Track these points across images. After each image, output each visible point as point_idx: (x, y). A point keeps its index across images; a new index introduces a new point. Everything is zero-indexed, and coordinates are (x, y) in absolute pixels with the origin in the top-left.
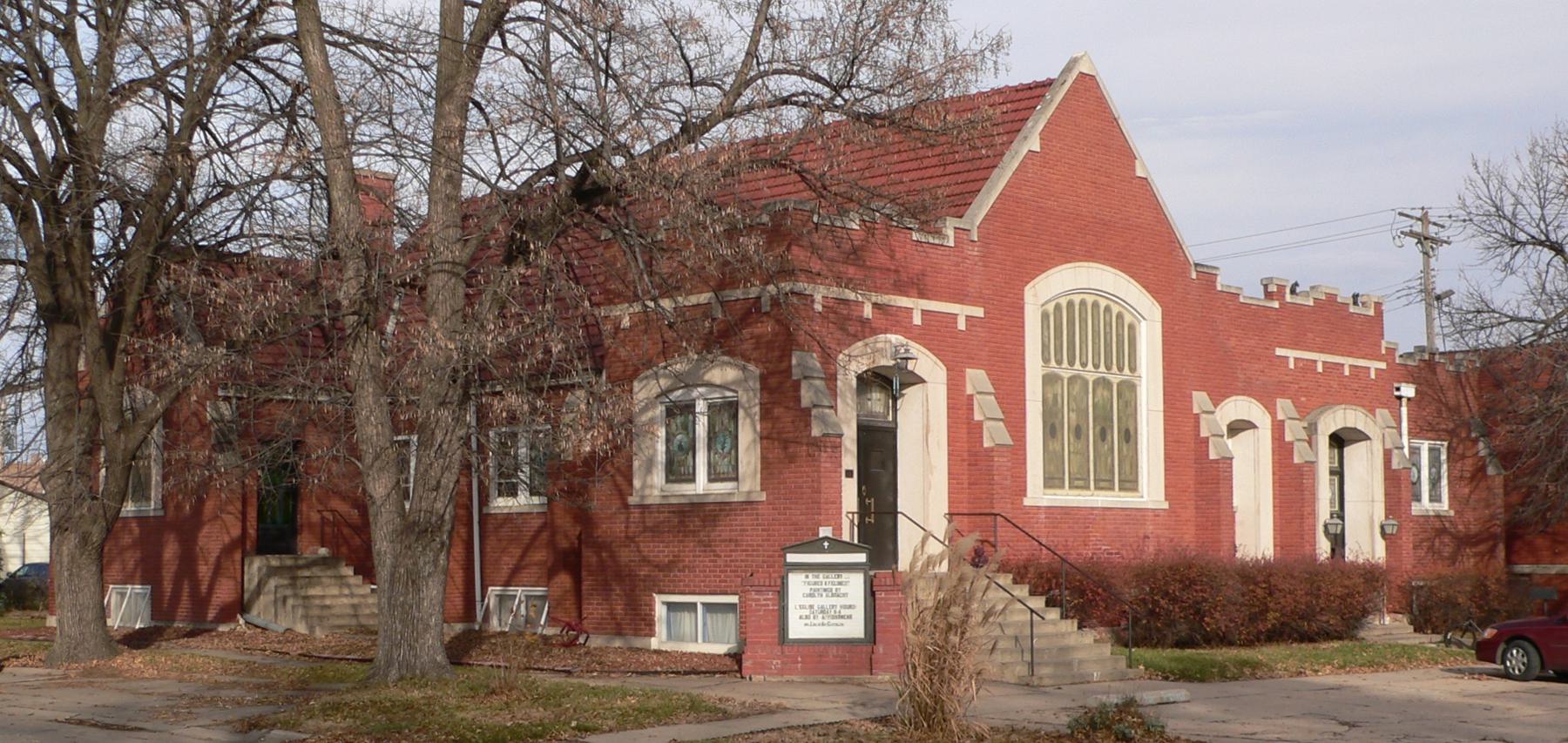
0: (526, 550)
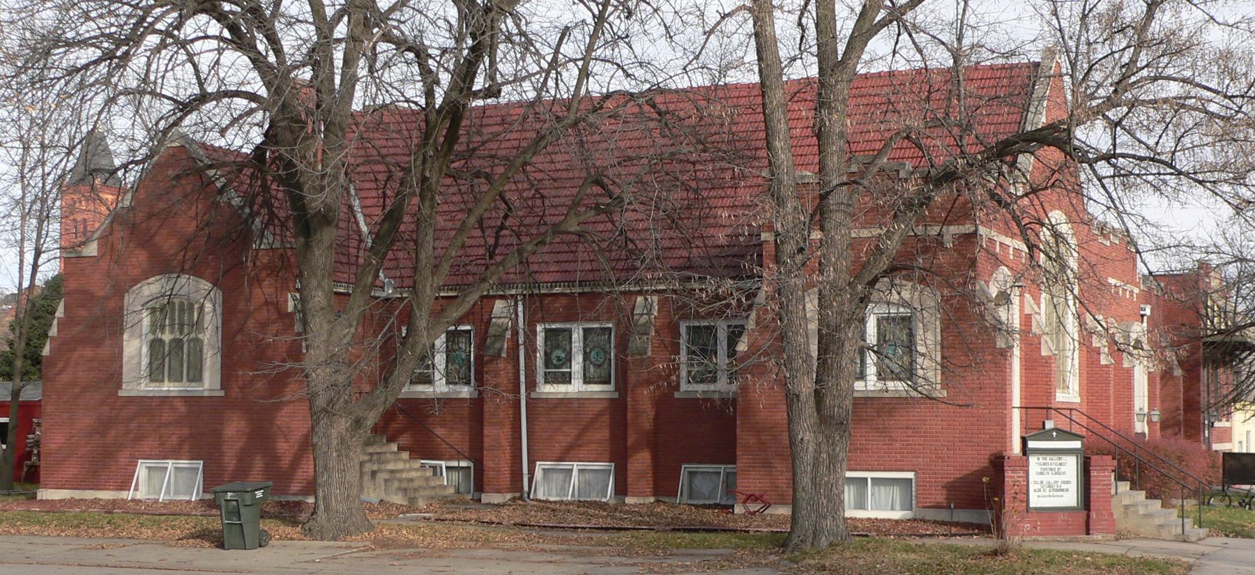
0: (585, 430)
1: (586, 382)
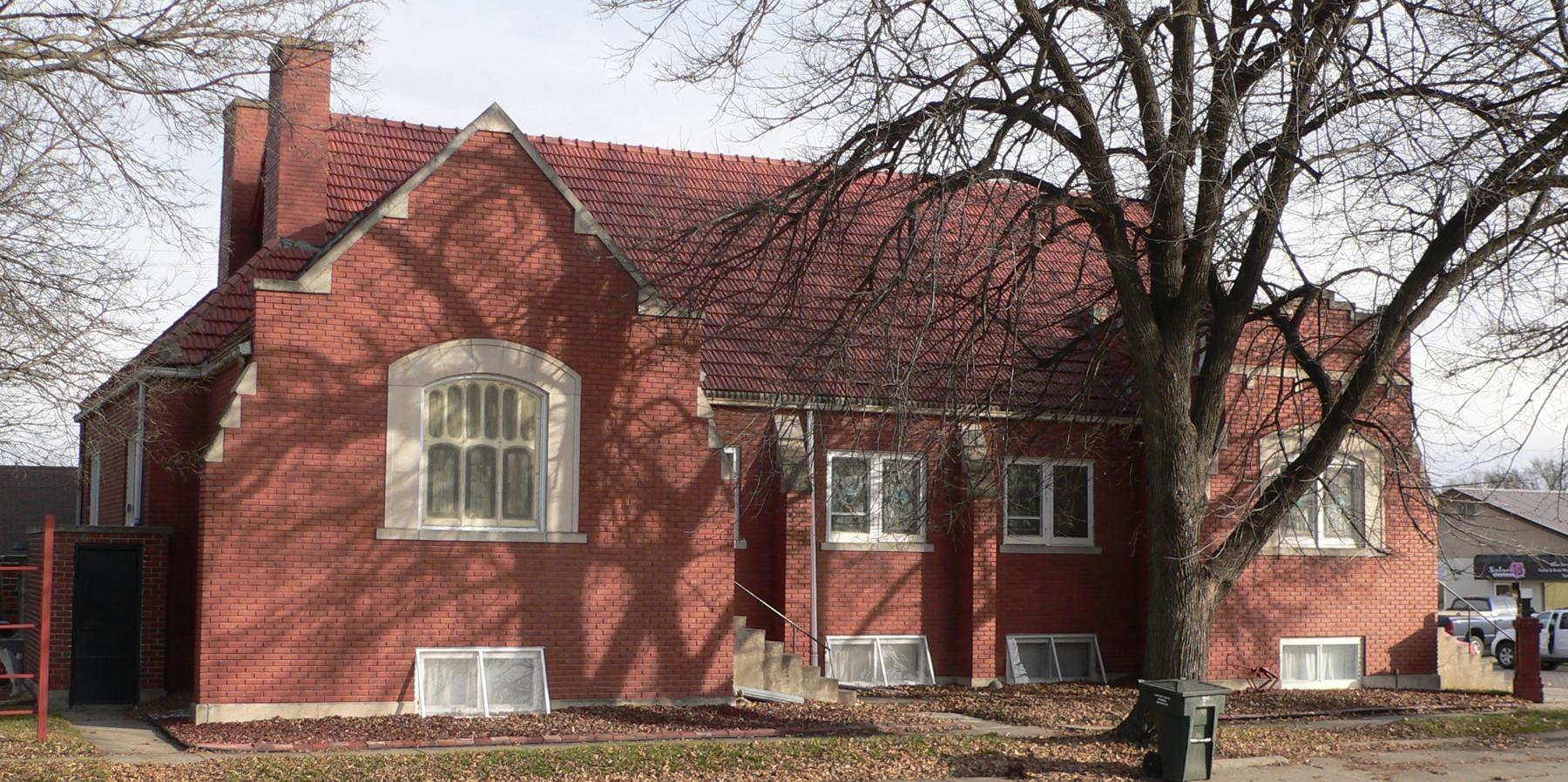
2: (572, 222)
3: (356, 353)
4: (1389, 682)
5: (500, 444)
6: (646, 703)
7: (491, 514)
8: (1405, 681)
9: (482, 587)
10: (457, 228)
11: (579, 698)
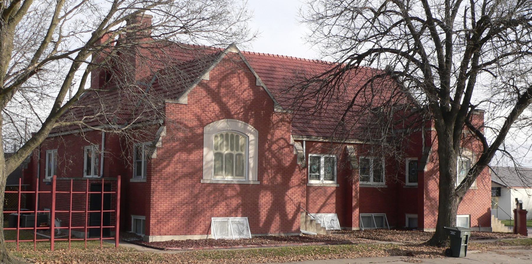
1: (374, 181)
2: (256, 82)
3: (195, 123)
4: (478, 229)
5: (235, 153)
6: (276, 235)
7: (232, 175)
8: (482, 229)
9: (232, 197)
10: (224, 83)
11: (257, 233)
